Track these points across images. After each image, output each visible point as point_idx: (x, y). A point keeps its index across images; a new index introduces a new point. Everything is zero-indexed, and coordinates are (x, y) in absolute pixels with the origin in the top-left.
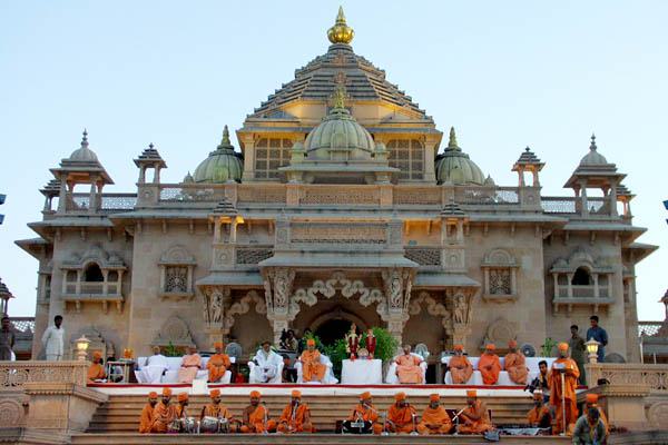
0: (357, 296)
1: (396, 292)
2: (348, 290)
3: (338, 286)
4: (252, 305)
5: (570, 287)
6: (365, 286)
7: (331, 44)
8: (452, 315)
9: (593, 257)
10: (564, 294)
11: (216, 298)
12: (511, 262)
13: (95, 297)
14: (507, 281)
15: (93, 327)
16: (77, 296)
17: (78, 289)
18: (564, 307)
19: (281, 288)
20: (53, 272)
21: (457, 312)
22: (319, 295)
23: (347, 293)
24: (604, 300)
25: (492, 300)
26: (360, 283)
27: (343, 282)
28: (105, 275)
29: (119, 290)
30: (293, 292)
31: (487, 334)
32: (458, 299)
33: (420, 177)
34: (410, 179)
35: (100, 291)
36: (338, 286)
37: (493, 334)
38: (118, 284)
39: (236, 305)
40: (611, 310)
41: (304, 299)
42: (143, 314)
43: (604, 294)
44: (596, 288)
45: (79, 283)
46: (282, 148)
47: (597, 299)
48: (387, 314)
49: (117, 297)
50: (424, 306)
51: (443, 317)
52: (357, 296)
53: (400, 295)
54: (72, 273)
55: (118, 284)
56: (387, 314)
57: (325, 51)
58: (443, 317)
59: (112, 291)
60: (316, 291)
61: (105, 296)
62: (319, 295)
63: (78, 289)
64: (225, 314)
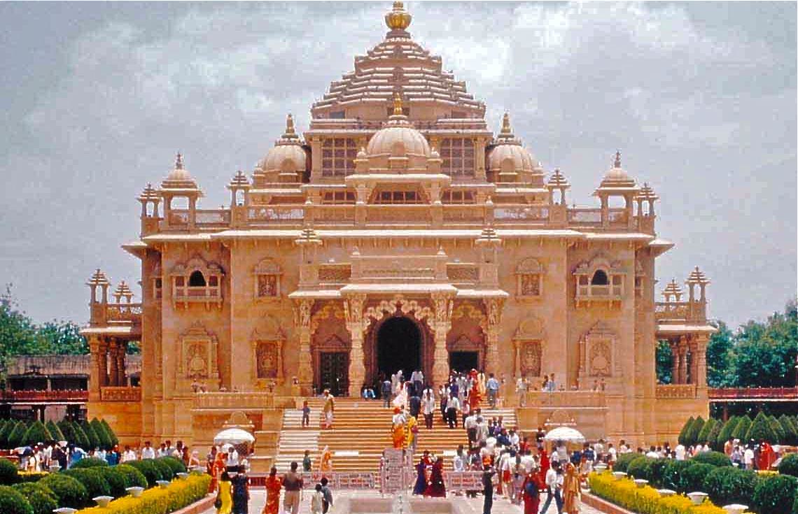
0: (412, 312)
1: (441, 309)
2: (406, 308)
3: (399, 306)
4: (332, 311)
5: (589, 287)
6: (418, 305)
7: (390, 30)
8: (487, 320)
9: (609, 261)
10: (584, 293)
11: (304, 308)
12: (538, 269)
13: (199, 299)
14: (536, 284)
15: (198, 322)
16: (185, 299)
17: (186, 293)
18: (584, 304)
19: (357, 308)
20: (163, 277)
21: (491, 317)
22: (385, 312)
23: (405, 310)
24: (617, 298)
25: (524, 300)
26: (416, 303)
27: (402, 302)
28: (207, 281)
29: (219, 292)
30: (365, 310)
31: (519, 328)
32: (492, 308)
33: (472, 174)
34: (363, 487)
35: (203, 293)
36: (399, 306)
37: (523, 328)
38: (218, 288)
39: (319, 312)
40: (622, 305)
41: (374, 315)
42: (240, 314)
43: (617, 292)
44: (611, 287)
45: (186, 288)
46: (345, 148)
47: (611, 296)
48: (435, 325)
49: (218, 299)
50: (466, 311)
51: (480, 320)
52: (412, 312)
53: (445, 312)
54: (180, 281)
55: (218, 288)
56: (435, 325)
57: (382, 38)
58: (480, 320)
59: (214, 293)
60: (382, 309)
61: (208, 298)
62: (385, 312)
63: (186, 293)
64: (311, 320)
